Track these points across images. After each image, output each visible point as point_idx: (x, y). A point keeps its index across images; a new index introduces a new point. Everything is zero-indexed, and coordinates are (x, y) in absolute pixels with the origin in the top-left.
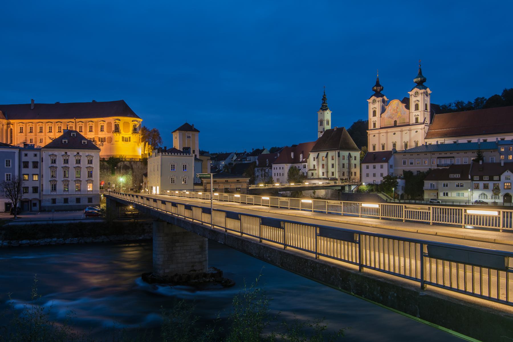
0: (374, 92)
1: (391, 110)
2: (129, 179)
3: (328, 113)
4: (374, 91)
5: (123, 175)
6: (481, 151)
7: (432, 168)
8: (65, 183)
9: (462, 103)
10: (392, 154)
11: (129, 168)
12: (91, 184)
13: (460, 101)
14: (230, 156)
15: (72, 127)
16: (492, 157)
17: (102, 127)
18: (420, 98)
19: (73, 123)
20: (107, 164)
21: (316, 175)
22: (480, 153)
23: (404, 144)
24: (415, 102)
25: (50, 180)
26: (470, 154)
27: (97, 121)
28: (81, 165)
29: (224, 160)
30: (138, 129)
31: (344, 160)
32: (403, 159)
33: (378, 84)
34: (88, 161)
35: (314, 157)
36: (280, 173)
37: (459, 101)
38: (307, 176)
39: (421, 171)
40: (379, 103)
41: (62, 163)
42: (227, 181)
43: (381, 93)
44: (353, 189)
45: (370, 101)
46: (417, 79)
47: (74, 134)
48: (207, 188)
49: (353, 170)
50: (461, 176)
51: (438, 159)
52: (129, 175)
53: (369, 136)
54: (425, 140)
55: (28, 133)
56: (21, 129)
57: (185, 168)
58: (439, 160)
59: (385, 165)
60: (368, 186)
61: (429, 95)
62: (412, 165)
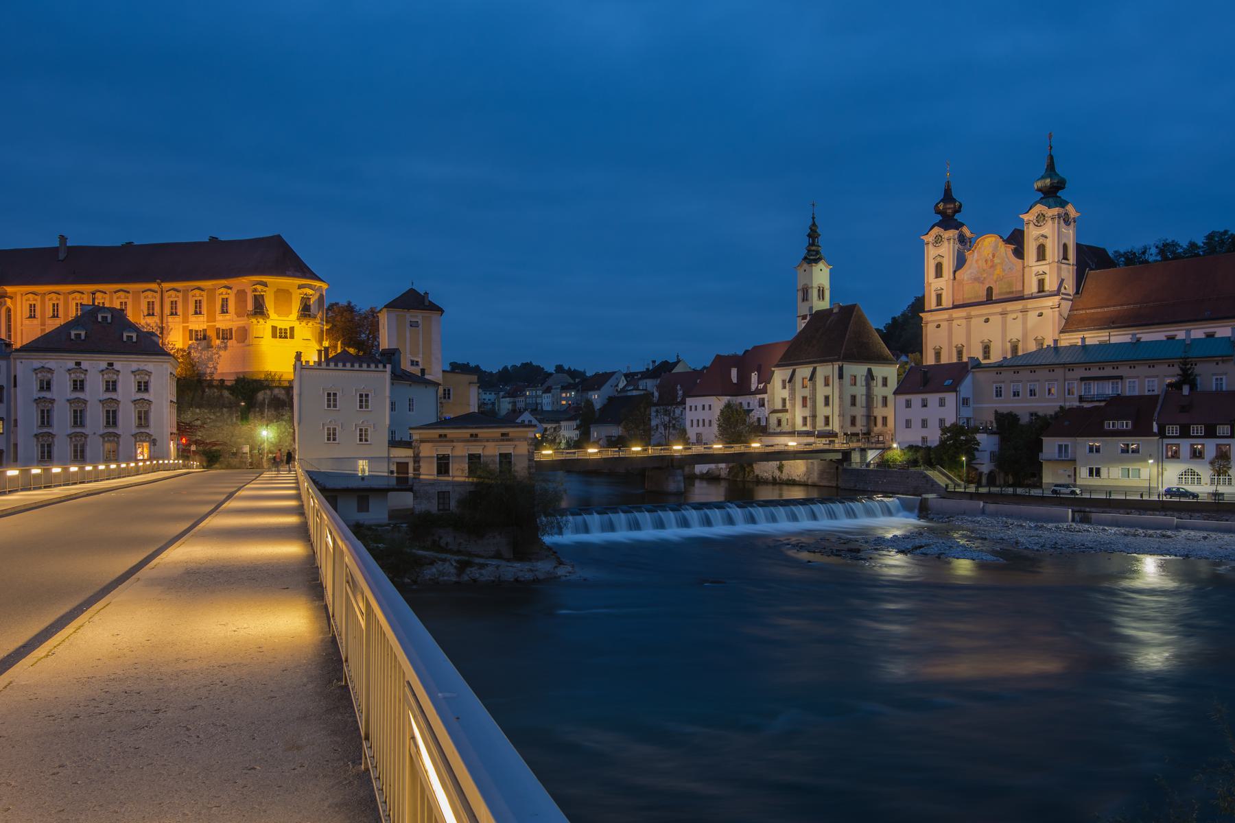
0: (939, 218)
1: (980, 262)
2: (284, 432)
3: (821, 270)
4: (938, 213)
5: (269, 422)
6: (1190, 360)
7: (1067, 405)
8: (76, 440)
9: (1174, 245)
10: (968, 371)
11: (286, 403)
12: (144, 444)
13: (1169, 241)
14: (612, 381)
15: (153, 302)
16: (1218, 377)
17: (225, 301)
18: (1048, 229)
19: (155, 294)
20: (230, 394)
21: (787, 424)
22: (1189, 366)
23: (1009, 345)
24: (1037, 239)
25: (36, 433)
26: (1162, 369)
27: (211, 287)
28: (119, 395)
29: (599, 389)
30: (313, 309)
31: (854, 387)
32: (994, 382)
33: (948, 197)
34: (138, 386)
35: (784, 378)
36: (704, 420)
37: (1168, 242)
38: (766, 426)
39: (1040, 414)
40: (949, 243)
42: (476, 435)
43: (956, 220)
44: (871, 460)
45: (929, 238)
46: (1043, 181)
47: (106, 317)
48: (421, 455)
49: (879, 412)
50: (1133, 425)
51: (1083, 383)
52: (284, 423)
53: (927, 326)
54: (1061, 335)
55: (47, 319)
56: (32, 308)
57: (364, 399)
58: (1085, 384)
59: (950, 398)
60: (906, 451)
61: (1072, 223)
62: (1016, 398)
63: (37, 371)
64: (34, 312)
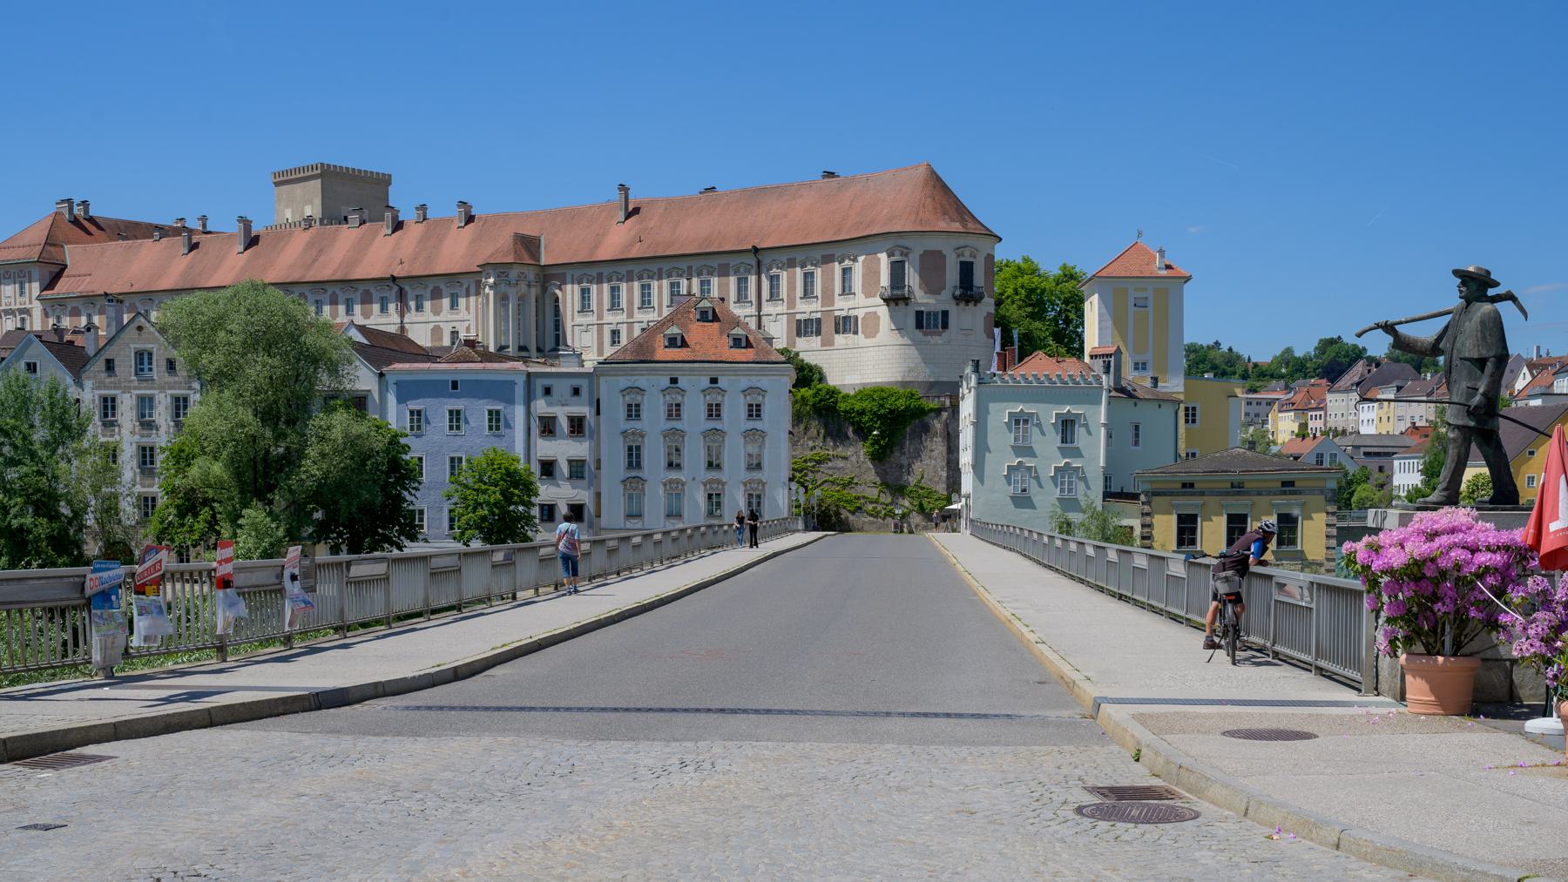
28: (725, 423)
41: (662, 415)
63: (624, 393)
64: (589, 300)
